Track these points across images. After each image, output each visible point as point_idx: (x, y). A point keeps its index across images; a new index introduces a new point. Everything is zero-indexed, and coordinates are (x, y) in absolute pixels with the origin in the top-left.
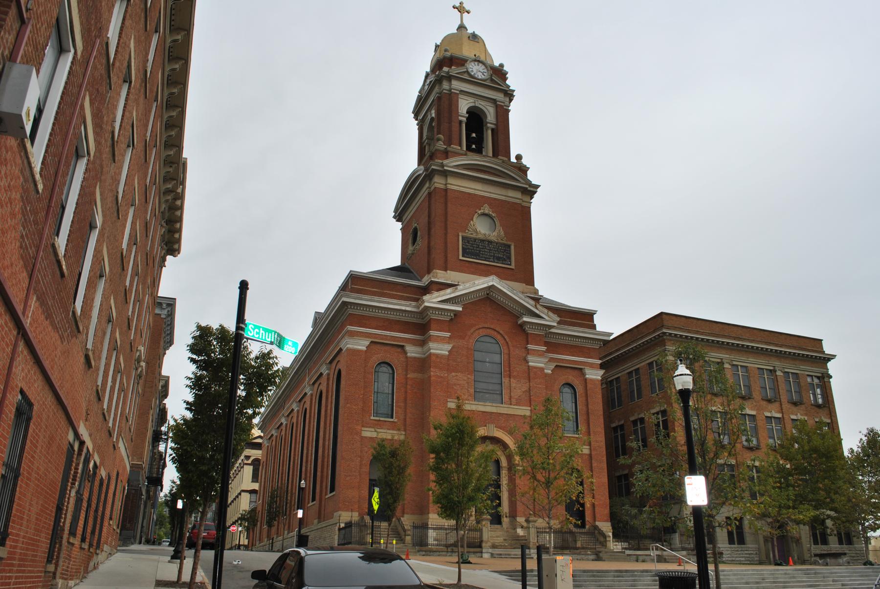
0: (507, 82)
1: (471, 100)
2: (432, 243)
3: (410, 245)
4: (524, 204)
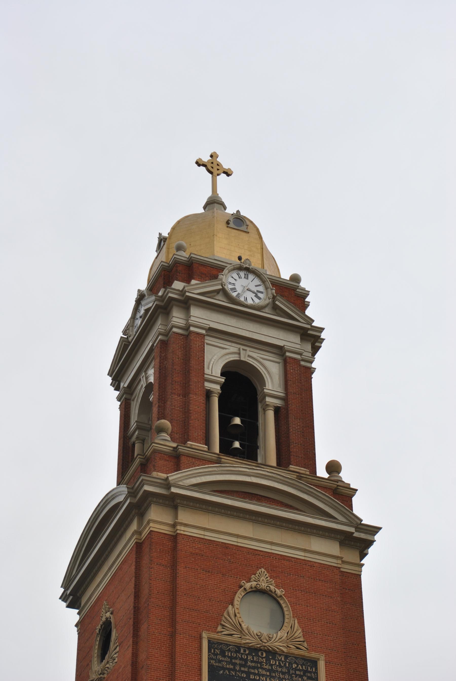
0: (308, 312)
1: (232, 348)
2: (142, 656)
3: (95, 660)
4: (347, 568)
